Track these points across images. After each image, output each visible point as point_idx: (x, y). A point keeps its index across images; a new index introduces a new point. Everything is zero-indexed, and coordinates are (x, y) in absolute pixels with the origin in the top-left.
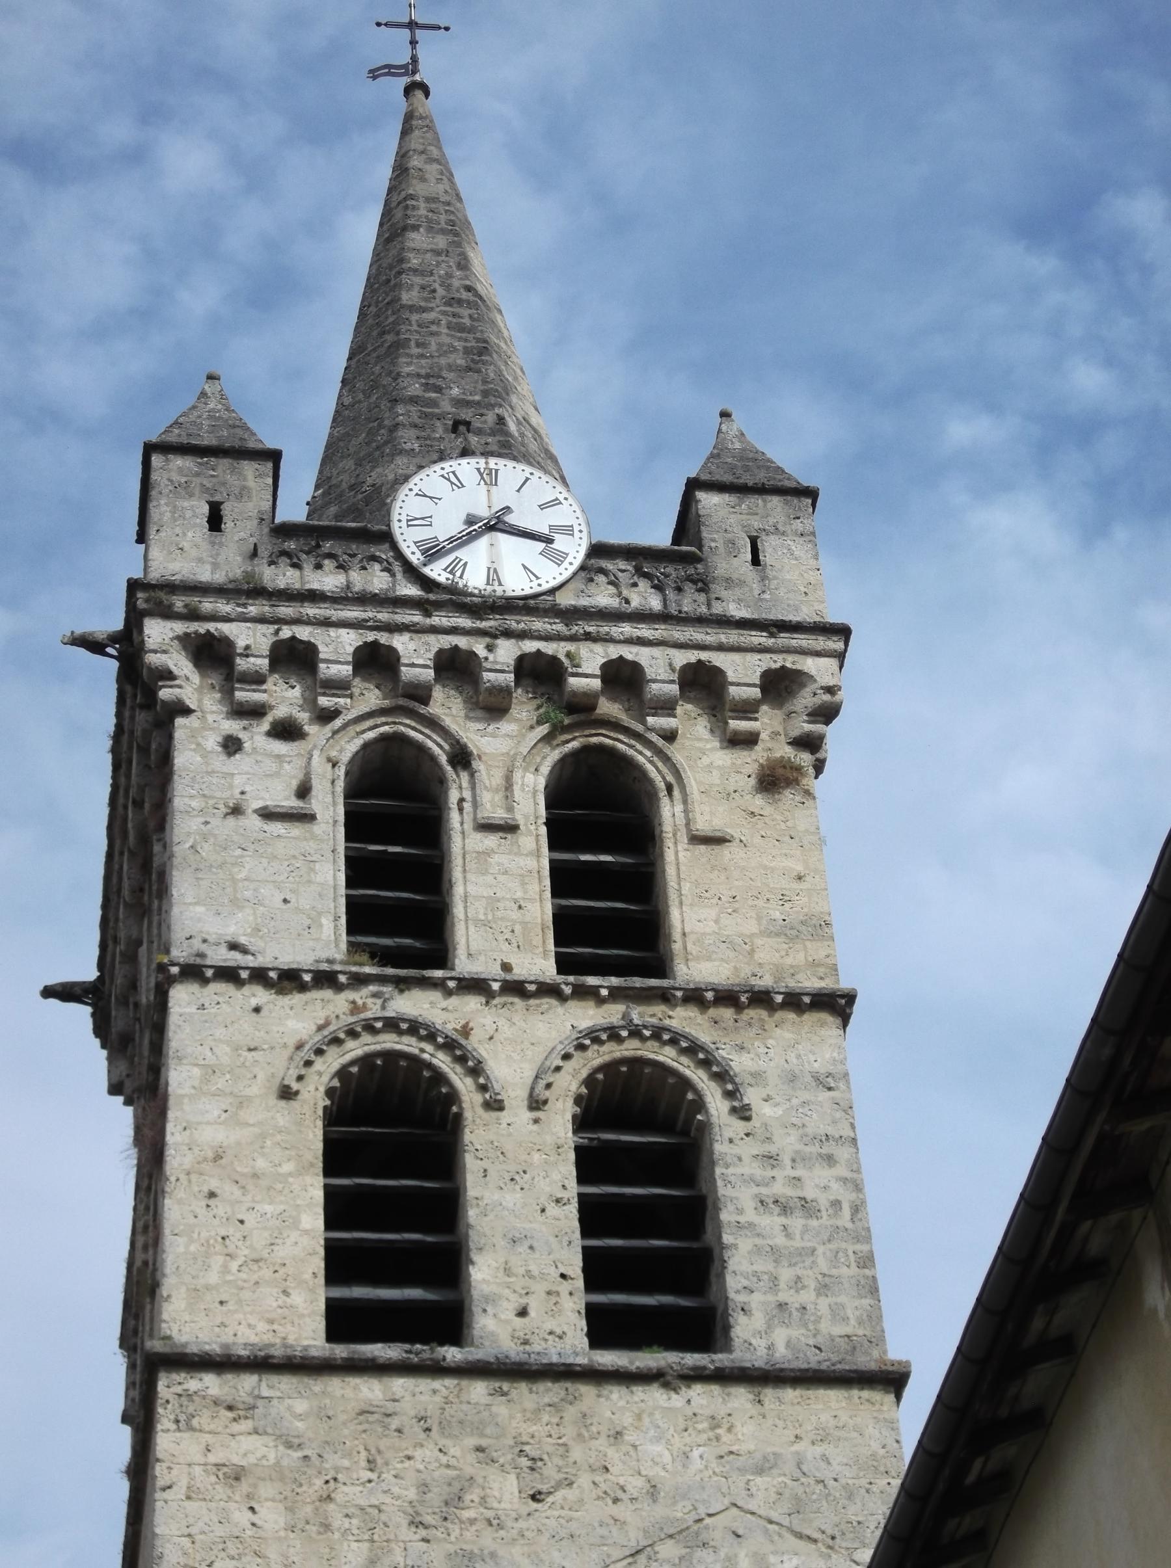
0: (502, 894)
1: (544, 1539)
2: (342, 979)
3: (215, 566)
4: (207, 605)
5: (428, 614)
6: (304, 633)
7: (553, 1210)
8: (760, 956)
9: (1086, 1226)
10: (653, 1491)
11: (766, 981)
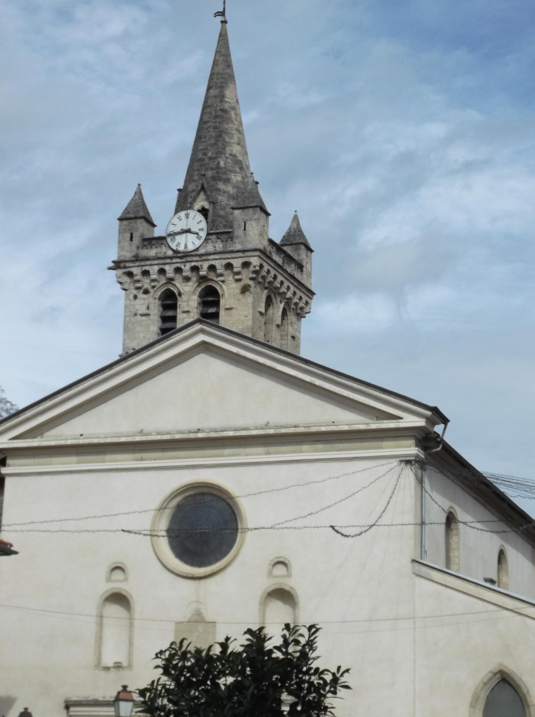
4: (128, 264)
5: (171, 260)
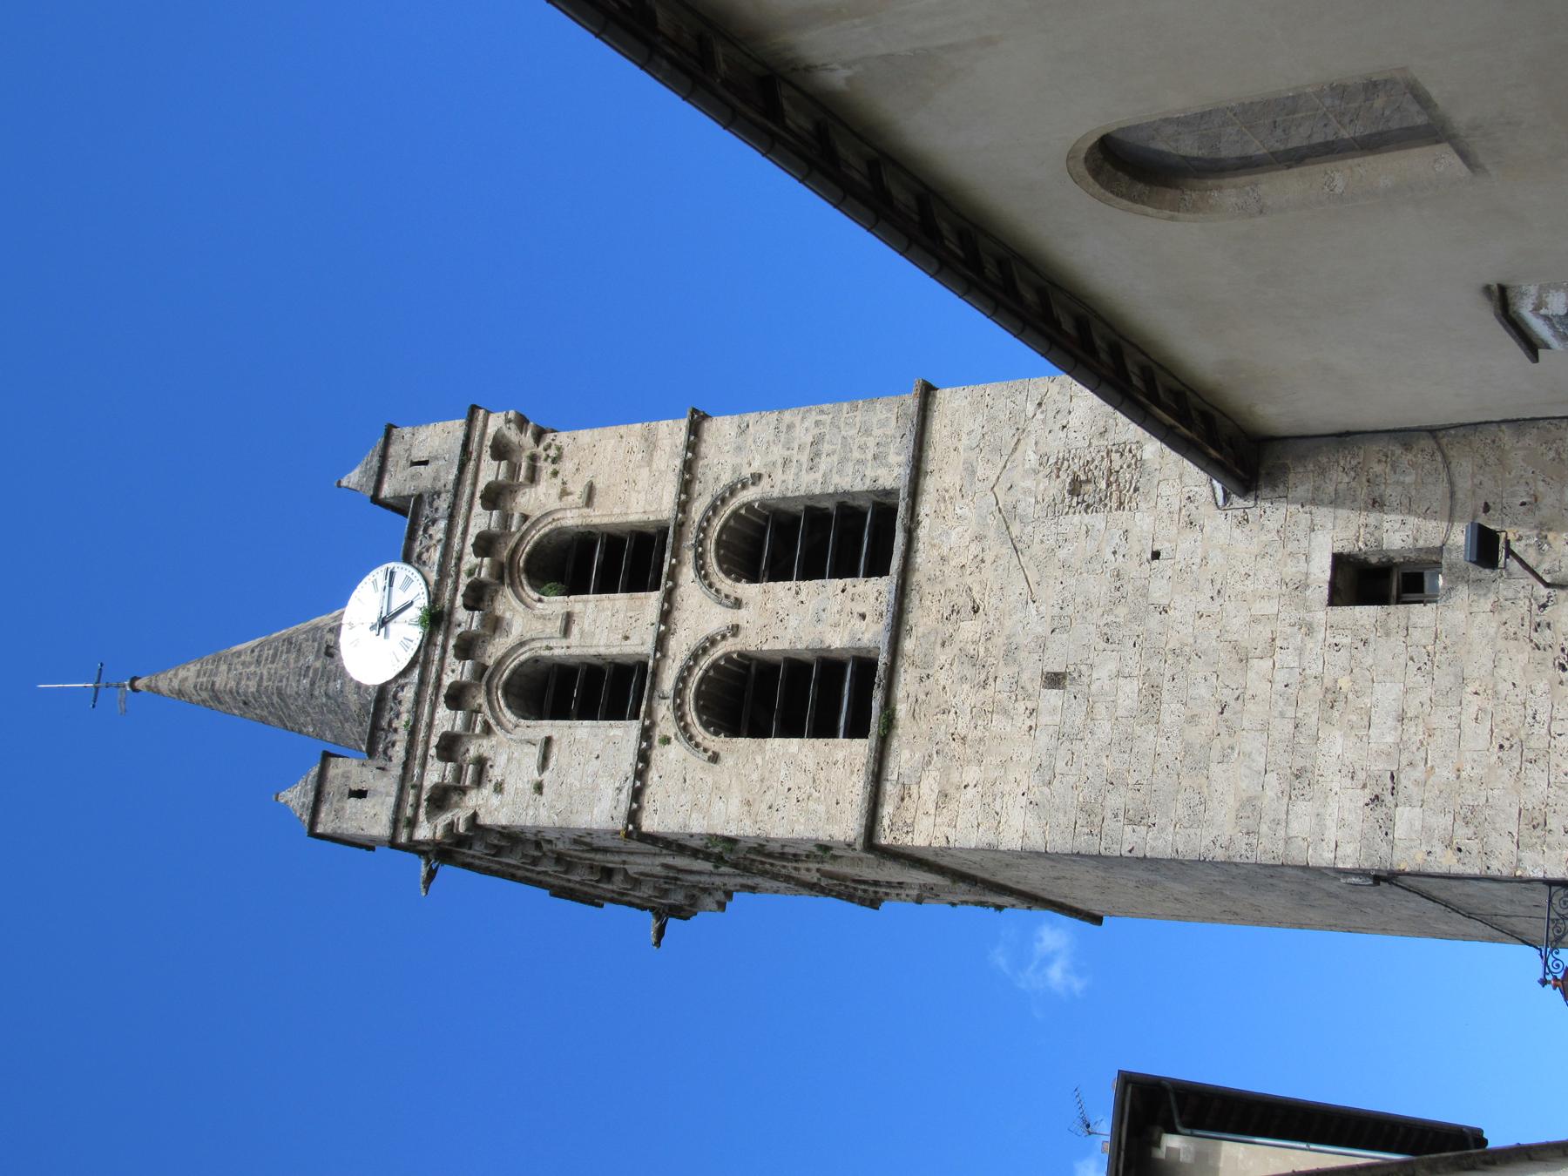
0: (608, 625)
1: (1001, 606)
2: (647, 723)
3: (388, 794)
6: (434, 740)
7: (803, 597)
8: (663, 467)
9: (788, 122)
10: (979, 538)
11: (678, 463)
